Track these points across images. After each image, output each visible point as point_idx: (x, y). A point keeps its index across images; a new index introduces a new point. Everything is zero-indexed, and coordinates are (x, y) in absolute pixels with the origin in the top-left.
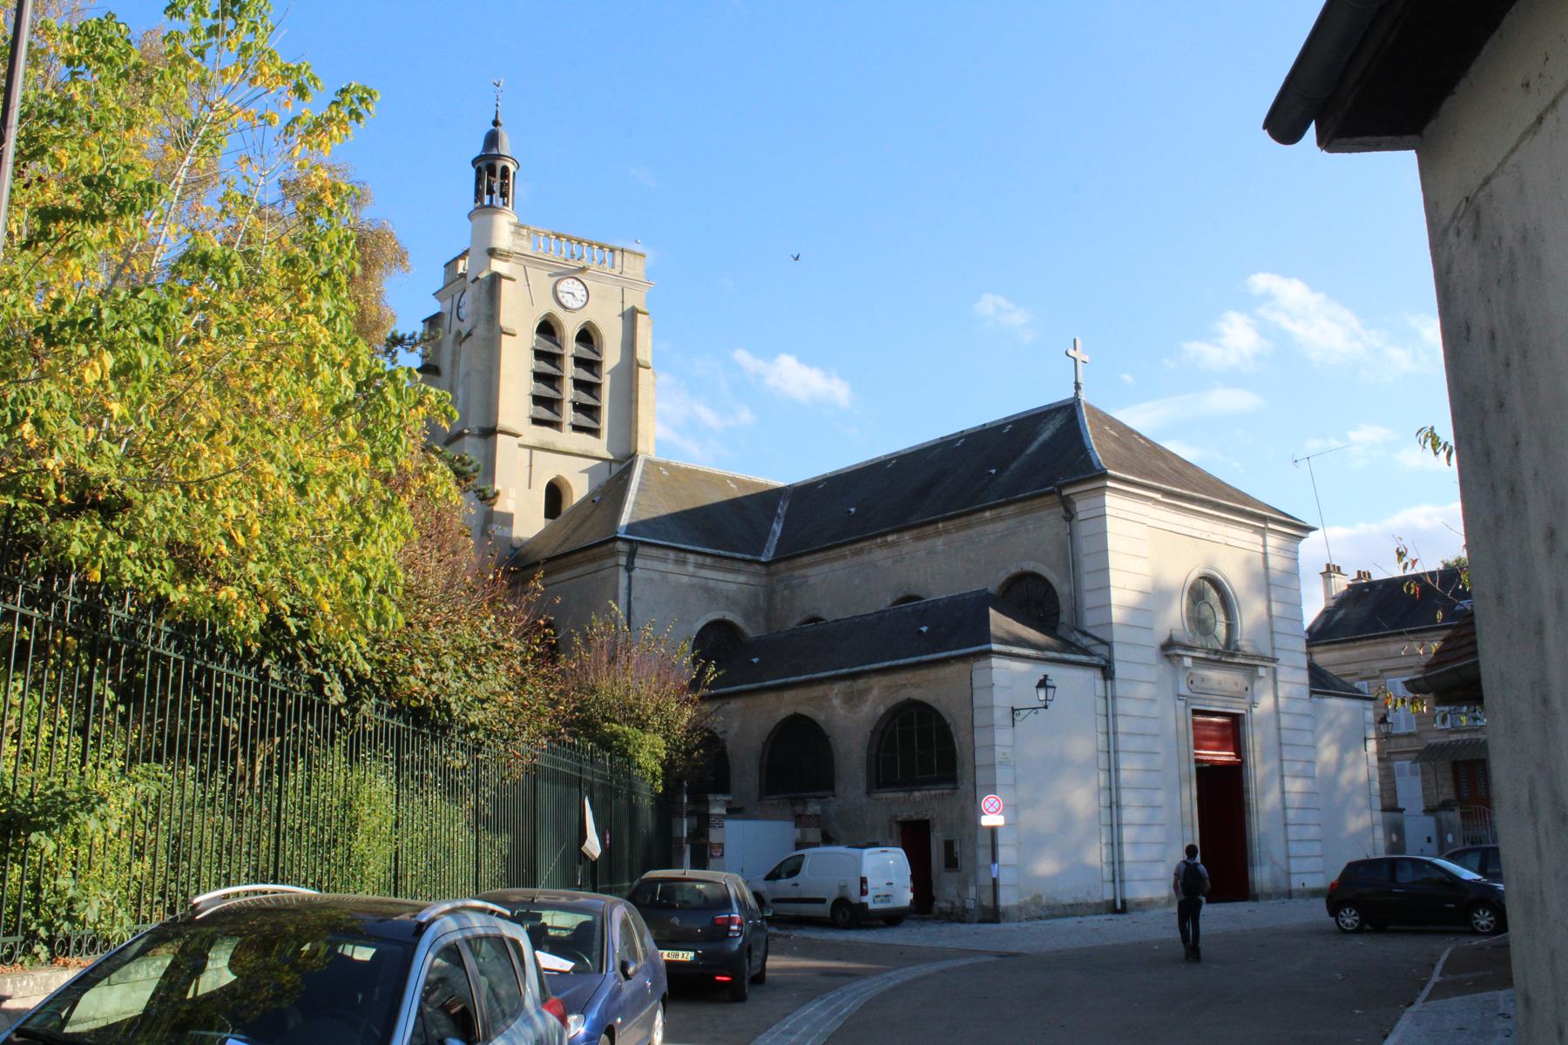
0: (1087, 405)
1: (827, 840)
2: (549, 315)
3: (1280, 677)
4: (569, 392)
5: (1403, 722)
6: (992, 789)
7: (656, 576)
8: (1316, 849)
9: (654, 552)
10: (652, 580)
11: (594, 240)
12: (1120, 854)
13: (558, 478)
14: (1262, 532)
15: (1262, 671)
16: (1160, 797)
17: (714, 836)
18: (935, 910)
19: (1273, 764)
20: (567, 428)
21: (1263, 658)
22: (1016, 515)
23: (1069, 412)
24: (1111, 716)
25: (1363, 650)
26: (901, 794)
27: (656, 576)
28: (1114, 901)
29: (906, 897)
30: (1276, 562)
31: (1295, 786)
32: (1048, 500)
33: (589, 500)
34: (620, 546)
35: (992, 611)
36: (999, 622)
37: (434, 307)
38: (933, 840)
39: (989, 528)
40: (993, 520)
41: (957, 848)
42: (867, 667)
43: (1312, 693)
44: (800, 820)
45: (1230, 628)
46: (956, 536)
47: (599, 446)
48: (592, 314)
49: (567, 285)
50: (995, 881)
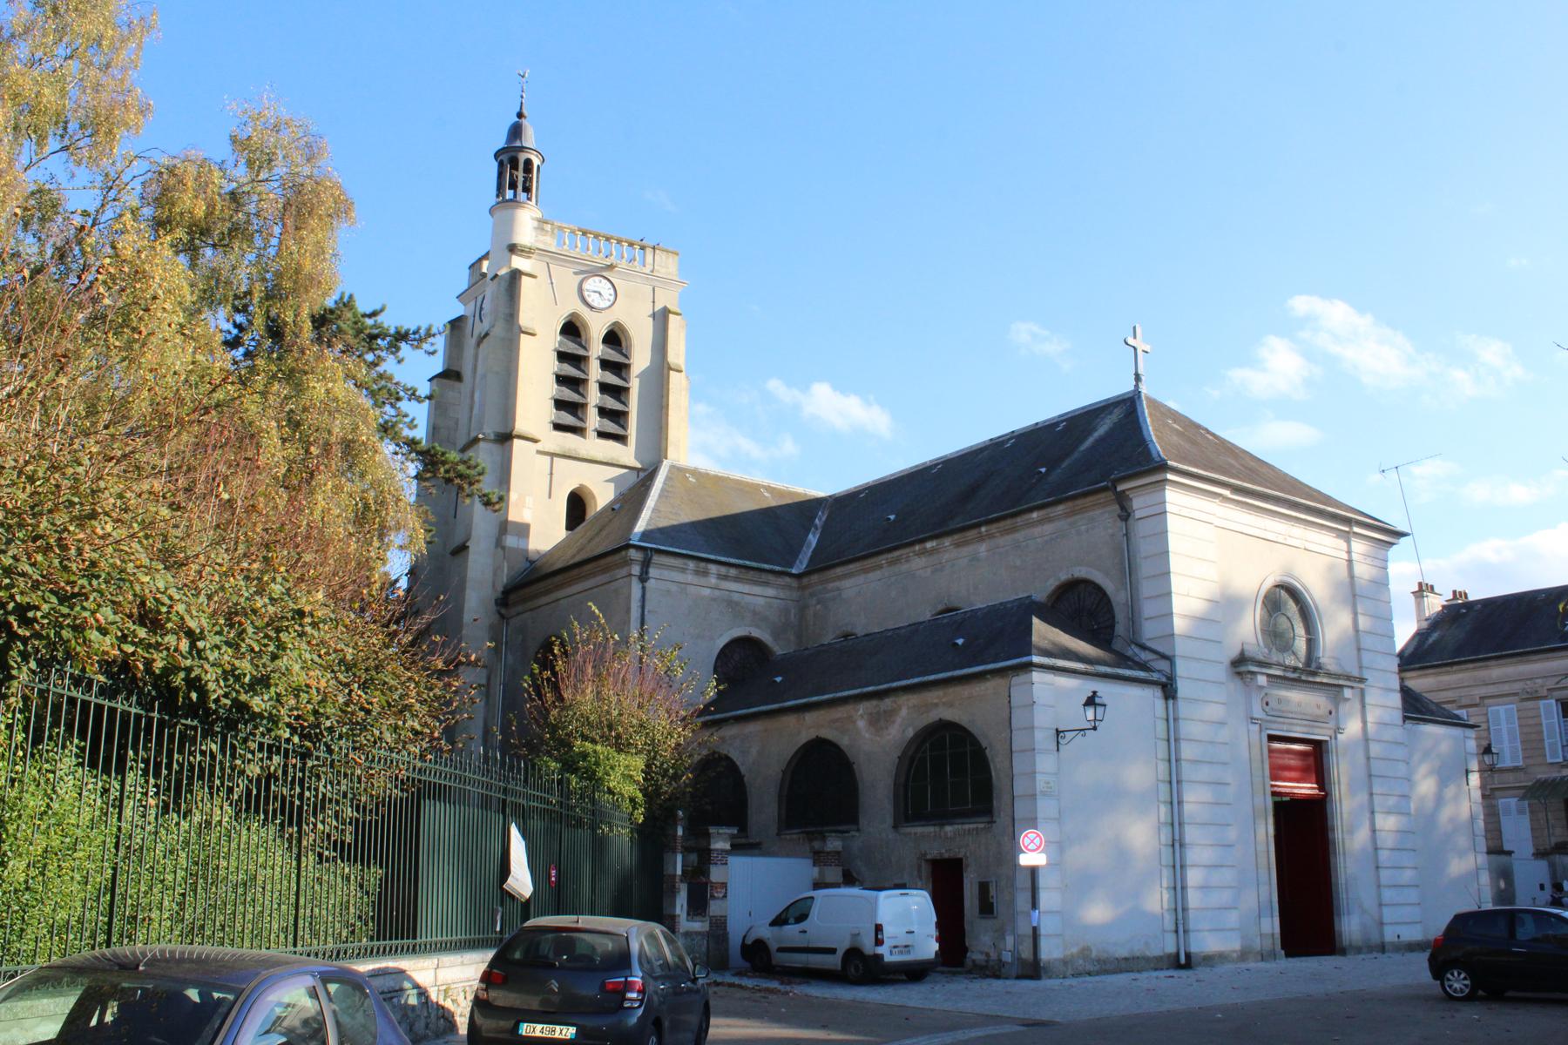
0: (1148, 399)
1: (849, 880)
2: (573, 315)
3: (1368, 700)
4: (594, 397)
6: (1033, 822)
7: (674, 588)
11: (624, 237)
12: (1184, 898)
13: (581, 487)
14: (1347, 536)
15: (1347, 693)
17: (716, 874)
18: (968, 963)
19: (1362, 797)
20: (591, 434)
21: (1348, 678)
23: (1128, 406)
24: (1173, 739)
25: (1460, 675)
26: (931, 829)
28: (1178, 955)
29: (929, 948)
30: (1363, 570)
31: (1388, 823)
32: (1102, 497)
33: (611, 508)
34: (633, 553)
35: (1035, 620)
36: (1043, 632)
37: (458, 310)
38: (965, 881)
39: (1037, 531)
40: (1041, 522)
41: (992, 892)
42: (895, 684)
43: (1405, 718)
44: (819, 858)
45: (1311, 643)
47: (627, 454)
48: (619, 314)
49: (593, 284)
50: (1035, 929)
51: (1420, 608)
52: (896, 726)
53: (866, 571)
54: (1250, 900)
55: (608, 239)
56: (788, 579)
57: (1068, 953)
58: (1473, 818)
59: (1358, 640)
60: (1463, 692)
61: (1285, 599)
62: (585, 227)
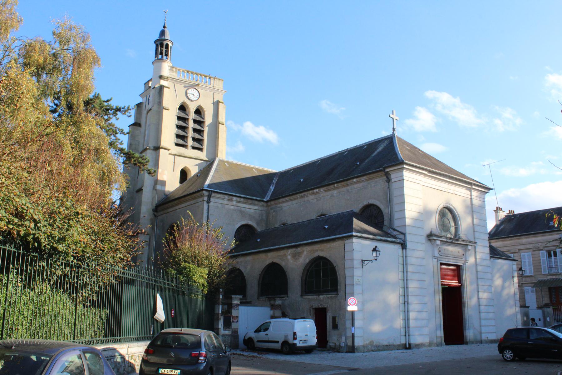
0: (397, 137)
1: (284, 315)
3: (477, 250)
4: (191, 133)
5: (528, 271)
6: (352, 295)
7: (220, 205)
8: (493, 323)
11: (203, 74)
13: (186, 167)
14: (470, 190)
15: (470, 247)
16: (426, 299)
17: (234, 313)
18: (328, 347)
19: (475, 286)
20: (189, 147)
21: (470, 242)
22: (366, 180)
23: (390, 140)
24: (405, 264)
25: (511, 242)
26: (315, 297)
27: (220, 205)
28: (406, 344)
29: (313, 341)
30: (476, 202)
31: (484, 296)
32: (380, 174)
33: (196, 175)
34: (204, 192)
35: (354, 219)
36: (357, 223)
37: (140, 100)
38: (327, 316)
39: (356, 186)
40: (357, 182)
41: (337, 320)
43: (491, 257)
44: (273, 307)
45: (456, 229)
46: (342, 189)
47: (203, 155)
49: (191, 91)
50: (353, 334)
51: (497, 216)
53: (292, 200)
54: (432, 325)
56: (262, 203)
58: (515, 294)
60: (512, 248)
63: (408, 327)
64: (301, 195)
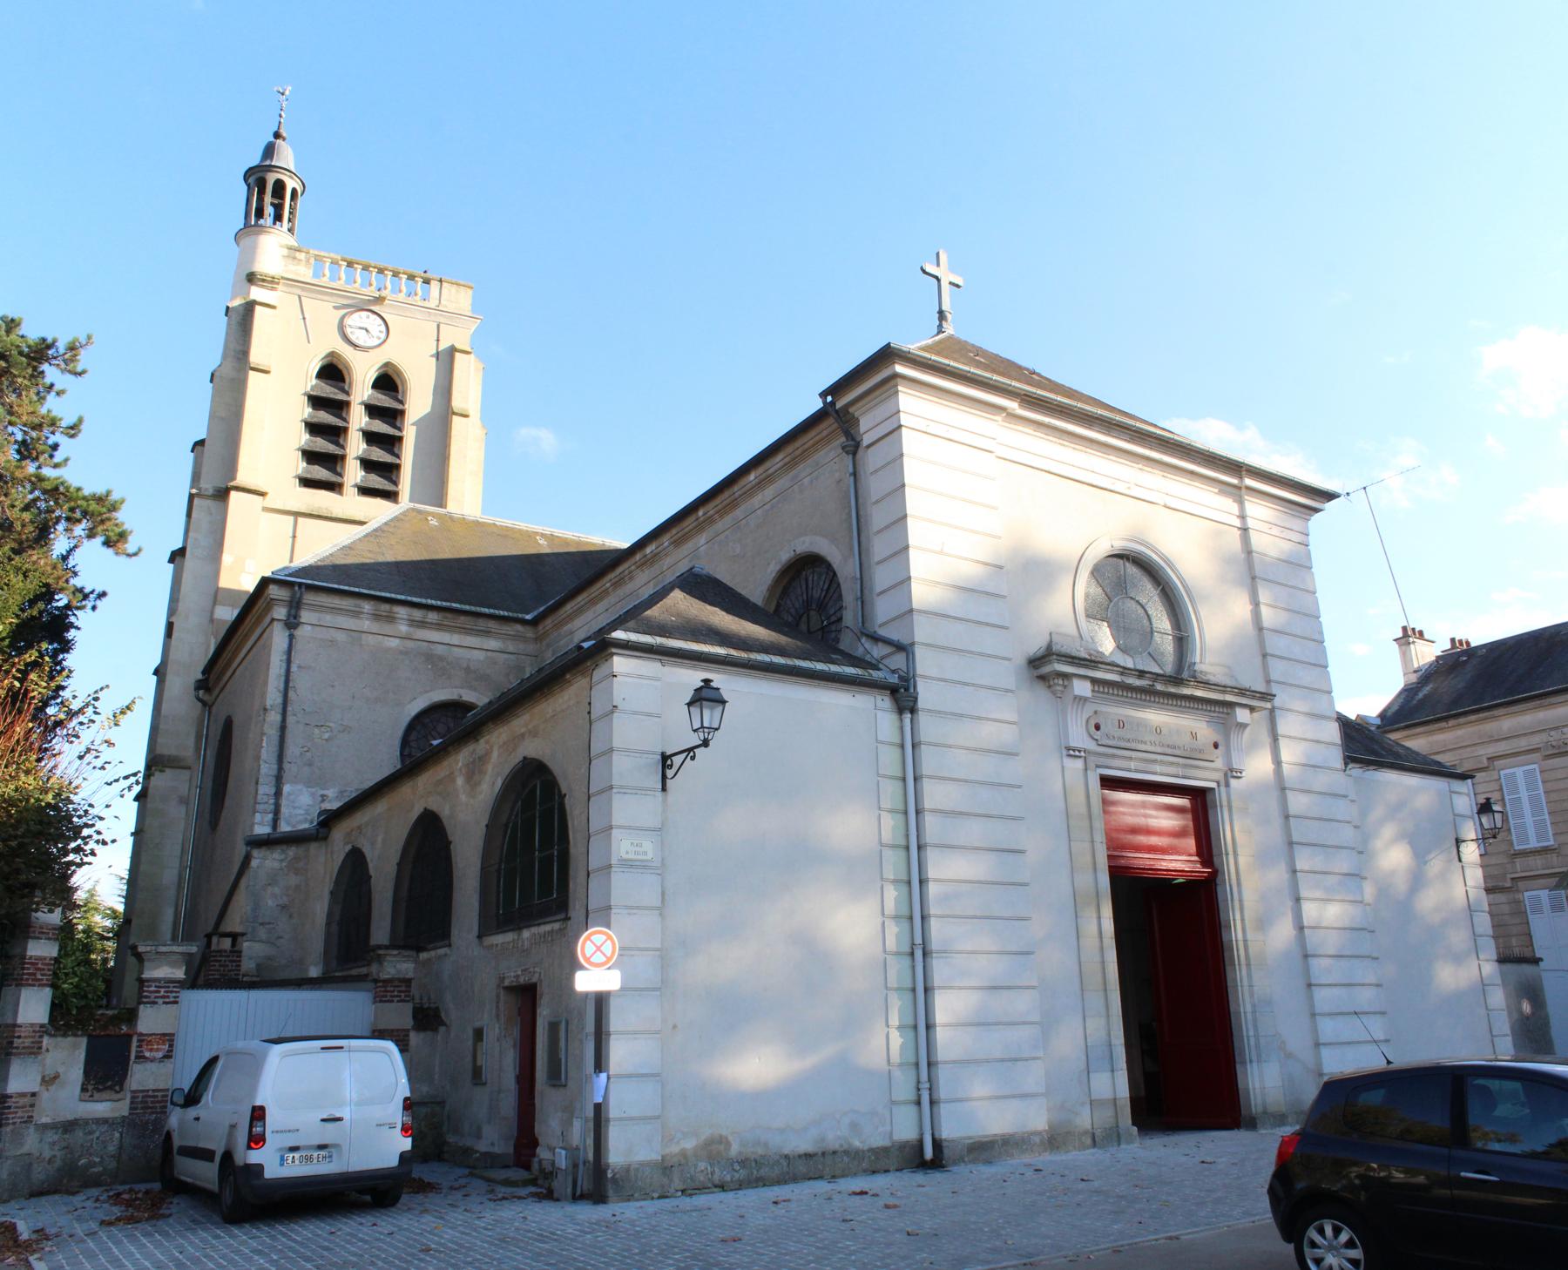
2: (332, 354)
3: (1283, 727)
4: (356, 446)
5: (1531, 832)
7: (341, 637)
9: (336, 601)
10: (333, 642)
14: (1237, 493)
15: (1242, 715)
19: (1277, 875)
20: (350, 490)
21: (1242, 692)
24: (912, 779)
25: (1460, 732)
28: (921, 1142)
31: (1327, 913)
39: (757, 500)
45: (1182, 641)
46: (720, 525)
49: (357, 320)
51: (1405, 657)
52: (487, 778)
53: (593, 602)
54: (1068, 1042)
55: (381, 271)
56: (519, 627)
57: (674, 1149)
58: (1471, 909)
59: (1261, 642)
60: (1465, 753)
61: (1134, 572)
62: (349, 258)
63: (930, 1064)
64: (612, 575)
